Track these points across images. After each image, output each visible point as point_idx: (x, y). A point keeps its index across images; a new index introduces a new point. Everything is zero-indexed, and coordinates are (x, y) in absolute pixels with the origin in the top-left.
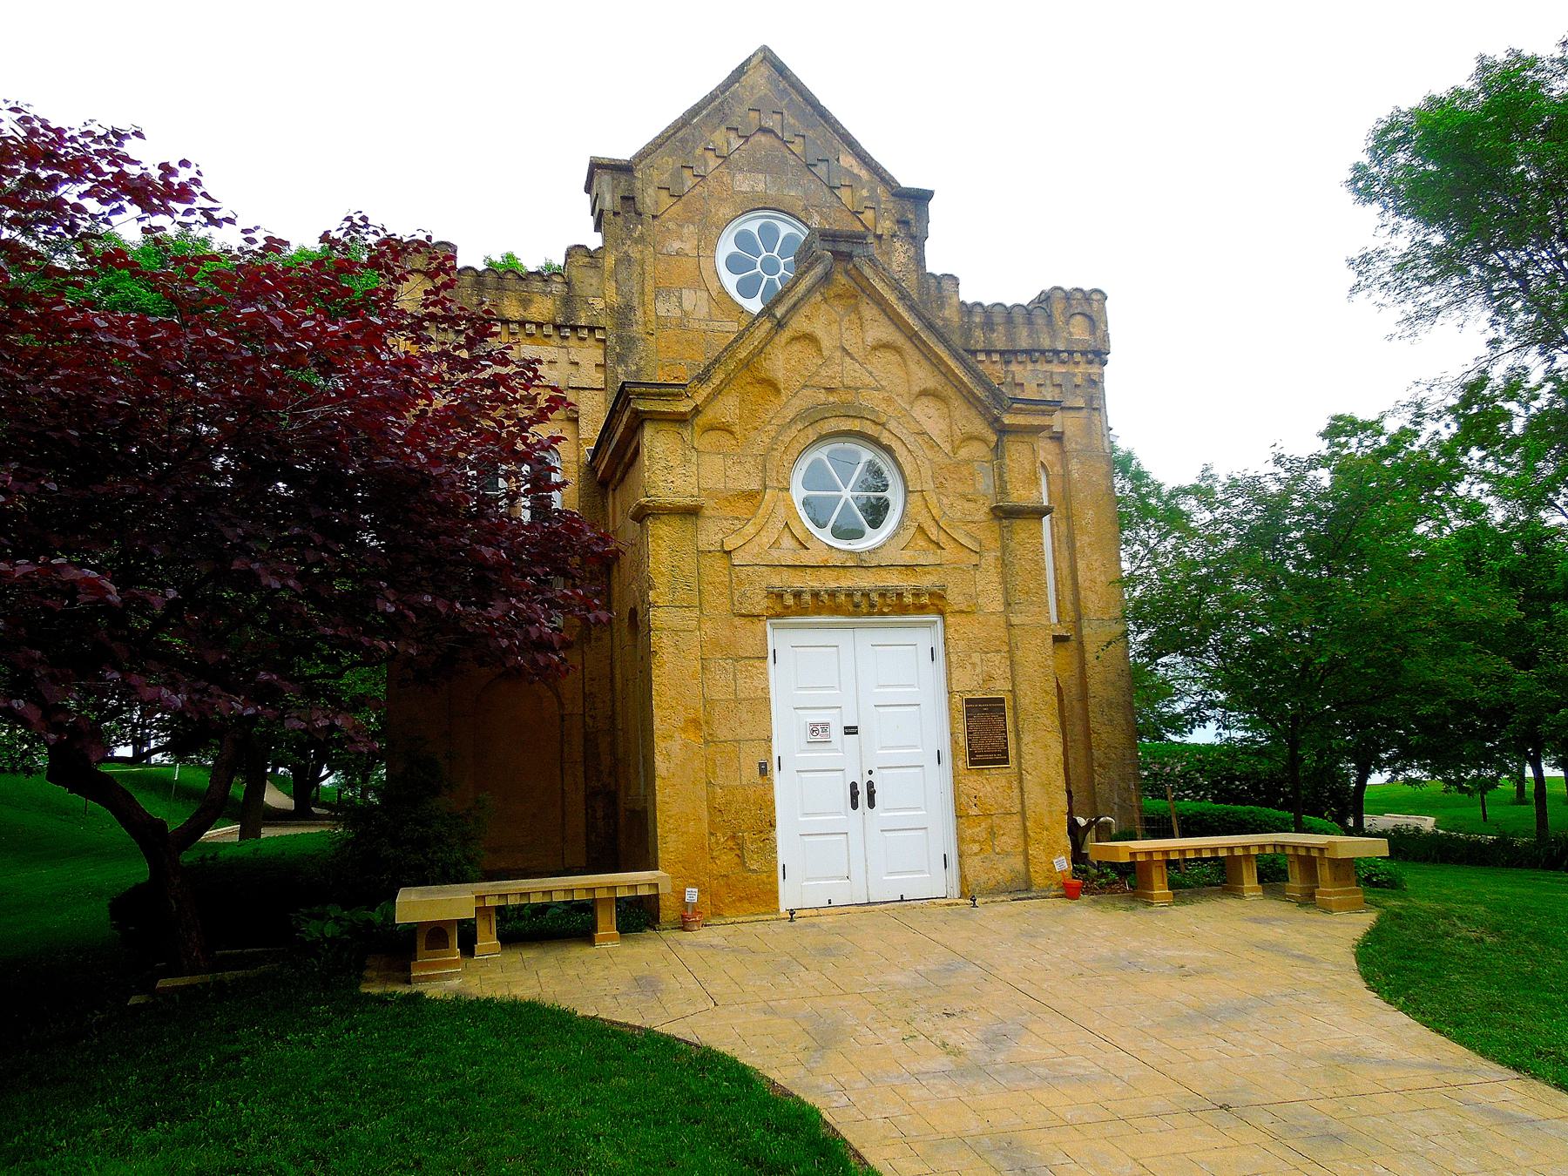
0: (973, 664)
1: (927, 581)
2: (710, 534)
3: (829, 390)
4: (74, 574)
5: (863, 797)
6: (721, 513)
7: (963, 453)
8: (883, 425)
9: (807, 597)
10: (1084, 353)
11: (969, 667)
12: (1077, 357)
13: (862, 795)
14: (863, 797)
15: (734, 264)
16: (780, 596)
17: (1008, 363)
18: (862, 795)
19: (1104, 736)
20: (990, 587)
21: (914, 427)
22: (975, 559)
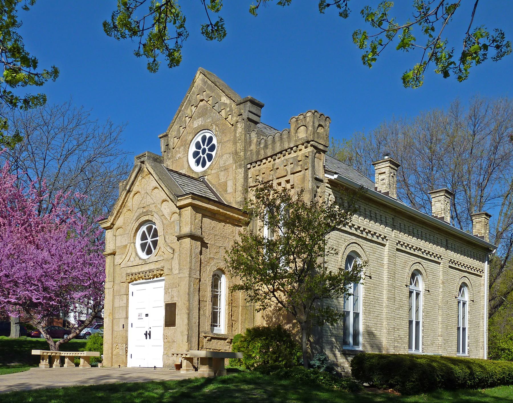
2: (118, 259)
15: (198, 162)
18: (148, 335)
21: (161, 214)
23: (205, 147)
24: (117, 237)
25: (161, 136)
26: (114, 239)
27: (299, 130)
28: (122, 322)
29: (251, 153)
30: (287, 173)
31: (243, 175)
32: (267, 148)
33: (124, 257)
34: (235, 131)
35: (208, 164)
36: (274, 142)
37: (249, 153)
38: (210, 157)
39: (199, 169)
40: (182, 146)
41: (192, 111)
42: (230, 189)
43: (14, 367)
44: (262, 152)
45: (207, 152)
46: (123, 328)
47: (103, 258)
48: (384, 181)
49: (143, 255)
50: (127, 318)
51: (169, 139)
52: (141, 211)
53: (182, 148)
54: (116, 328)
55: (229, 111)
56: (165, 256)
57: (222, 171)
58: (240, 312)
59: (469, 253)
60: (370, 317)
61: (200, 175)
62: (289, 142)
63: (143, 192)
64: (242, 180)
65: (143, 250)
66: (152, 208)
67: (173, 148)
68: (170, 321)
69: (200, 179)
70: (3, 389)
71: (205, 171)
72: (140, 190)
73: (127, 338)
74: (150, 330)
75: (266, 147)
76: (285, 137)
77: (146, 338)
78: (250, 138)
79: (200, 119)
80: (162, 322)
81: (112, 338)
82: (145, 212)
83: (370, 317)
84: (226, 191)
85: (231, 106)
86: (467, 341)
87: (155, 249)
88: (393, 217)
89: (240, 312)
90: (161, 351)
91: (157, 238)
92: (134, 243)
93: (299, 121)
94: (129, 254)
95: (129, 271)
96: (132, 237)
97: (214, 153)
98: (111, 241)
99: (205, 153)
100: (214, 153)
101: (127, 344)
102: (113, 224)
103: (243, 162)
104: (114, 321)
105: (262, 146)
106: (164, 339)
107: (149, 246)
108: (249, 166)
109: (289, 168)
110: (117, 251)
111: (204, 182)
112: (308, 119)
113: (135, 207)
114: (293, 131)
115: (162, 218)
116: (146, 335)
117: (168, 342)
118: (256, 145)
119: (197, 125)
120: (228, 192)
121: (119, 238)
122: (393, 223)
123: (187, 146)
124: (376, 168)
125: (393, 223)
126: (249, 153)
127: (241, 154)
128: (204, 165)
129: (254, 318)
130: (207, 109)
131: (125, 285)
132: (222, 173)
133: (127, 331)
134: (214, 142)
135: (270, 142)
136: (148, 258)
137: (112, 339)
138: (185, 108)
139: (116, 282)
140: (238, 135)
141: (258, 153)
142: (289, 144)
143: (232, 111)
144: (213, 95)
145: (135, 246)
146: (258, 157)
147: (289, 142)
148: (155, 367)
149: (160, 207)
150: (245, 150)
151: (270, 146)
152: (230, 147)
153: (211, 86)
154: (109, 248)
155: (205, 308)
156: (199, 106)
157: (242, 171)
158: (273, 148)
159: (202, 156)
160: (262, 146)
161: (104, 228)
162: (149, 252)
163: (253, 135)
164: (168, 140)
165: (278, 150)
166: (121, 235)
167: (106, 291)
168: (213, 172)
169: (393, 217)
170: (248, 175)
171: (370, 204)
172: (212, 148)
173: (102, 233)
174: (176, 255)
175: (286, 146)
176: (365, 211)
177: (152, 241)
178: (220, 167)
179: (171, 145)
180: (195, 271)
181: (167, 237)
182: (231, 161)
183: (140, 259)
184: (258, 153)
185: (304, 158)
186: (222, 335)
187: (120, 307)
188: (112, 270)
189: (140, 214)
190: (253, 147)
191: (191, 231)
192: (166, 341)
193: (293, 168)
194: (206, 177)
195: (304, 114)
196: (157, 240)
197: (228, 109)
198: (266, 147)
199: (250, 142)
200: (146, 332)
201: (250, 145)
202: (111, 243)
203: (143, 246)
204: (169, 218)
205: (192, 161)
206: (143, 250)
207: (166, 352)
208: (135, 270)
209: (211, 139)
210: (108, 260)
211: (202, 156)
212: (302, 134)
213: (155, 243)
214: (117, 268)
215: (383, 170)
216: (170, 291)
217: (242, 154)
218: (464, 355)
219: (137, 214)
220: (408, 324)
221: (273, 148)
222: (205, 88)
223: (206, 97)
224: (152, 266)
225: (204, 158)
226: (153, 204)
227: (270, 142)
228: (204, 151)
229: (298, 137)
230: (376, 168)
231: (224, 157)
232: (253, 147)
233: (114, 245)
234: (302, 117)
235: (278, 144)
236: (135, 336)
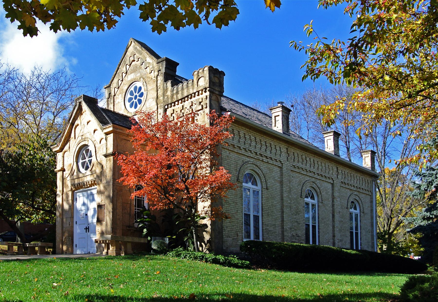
5: (87, 230)
15: (131, 106)
29: (167, 97)
32: (178, 94)
36: (183, 89)
37: (166, 97)
40: (120, 93)
43: (219, 294)
44: (175, 96)
55: (152, 68)
59: (358, 178)
62: (193, 89)
66: (88, 135)
75: (177, 93)
76: (190, 85)
78: (167, 87)
79: (132, 74)
85: (153, 64)
88: (287, 147)
103: (162, 104)
114: (195, 81)
122: (287, 152)
124: (272, 112)
125: (287, 152)
126: (166, 97)
128: (136, 107)
130: (137, 67)
134: (142, 90)
143: (154, 68)
144: (141, 56)
146: (172, 100)
147: (193, 89)
151: (180, 92)
153: (139, 51)
158: (182, 94)
160: (175, 92)
161: (55, 151)
165: (185, 94)
169: (287, 147)
171: (281, 143)
172: (141, 95)
175: (191, 92)
176: (261, 142)
177: (89, 160)
190: (169, 93)
197: (151, 67)
199: (167, 89)
201: (167, 92)
209: (140, 88)
221: (182, 94)
222: (135, 52)
225: (136, 102)
228: (136, 97)
230: (272, 112)
232: (169, 93)
235: (185, 91)
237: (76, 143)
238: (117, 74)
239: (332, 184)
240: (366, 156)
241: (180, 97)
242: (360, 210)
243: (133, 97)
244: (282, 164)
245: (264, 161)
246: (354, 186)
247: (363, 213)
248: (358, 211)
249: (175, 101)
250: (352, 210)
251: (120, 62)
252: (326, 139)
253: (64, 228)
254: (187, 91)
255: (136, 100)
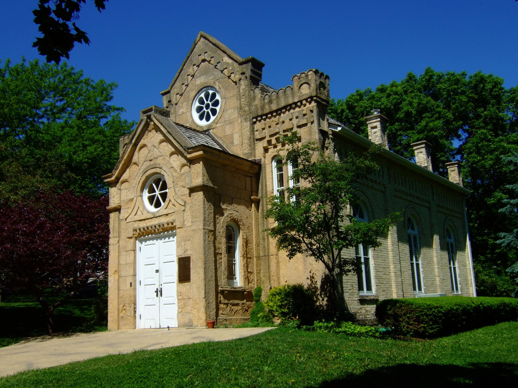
0: (182, 246)
1: (169, 219)
2: (124, 214)
3: (151, 160)
4: (504, 196)
5: (159, 293)
6: (126, 207)
7: (183, 171)
8: (161, 168)
9: (142, 230)
10: (306, 100)
11: (181, 247)
12: (304, 102)
13: (159, 292)
14: (159, 293)
15: (201, 118)
16: (136, 230)
17: (280, 115)
18: (159, 292)
19: (314, 266)
20: (188, 217)
21: (170, 166)
22: (183, 208)
23: (209, 102)
24: (122, 191)
25: (163, 92)
26: (119, 192)
27: (302, 87)
28: (130, 280)
30: (293, 125)
31: (249, 128)
33: (130, 211)
34: (239, 88)
35: (213, 118)
37: (253, 108)
38: (214, 112)
39: (203, 123)
41: (193, 70)
42: (236, 141)
44: (267, 107)
45: (211, 107)
46: (131, 286)
47: (107, 213)
48: (376, 134)
49: (152, 209)
50: (135, 275)
51: (172, 95)
52: (148, 163)
53: (185, 103)
54: (122, 287)
56: (176, 209)
57: (227, 124)
58: (255, 263)
60: (378, 261)
61: (205, 129)
62: (293, 98)
63: (149, 145)
64: (248, 133)
65: (151, 203)
67: (176, 104)
68: (184, 275)
69: (206, 132)
70: (4, 374)
71: (210, 126)
72: (147, 143)
73: (135, 297)
74: (161, 287)
77: (157, 296)
79: (203, 77)
80: (175, 277)
81: (118, 298)
82: (152, 165)
83: (378, 261)
84: (233, 144)
86: (458, 279)
87: (164, 201)
89: (255, 263)
90: (175, 309)
91: (167, 191)
92: (142, 196)
93: (302, 79)
94: (136, 208)
95: (137, 225)
96: (139, 190)
97: (218, 108)
98: (116, 196)
99: (208, 108)
100: (218, 108)
101: (135, 304)
102: (118, 179)
104: (121, 280)
105: (266, 101)
106: (178, 296)
107: (158, 198)
108: (254, 120)
109: (295, 122)
110: (122, 205)
111: (209, 135)
112: (310, 77)
113: (142, 160)
114: (296, 88)
115: (171, 170)
116: (157, 292)
117: (181, 298)
118: (261, 100)
119: (199, 83)
120: (235, 144)
121: (124, 192)
123: (191, 102)
127: (246, 108)
128: (208, 119)
129: (269, 268)
131: (132, 240)
132: (228, 127)
133: (135, 289)
134: (218, 97)
135: (274, 98)
136: (158, 211)
137: (118, 300)
138: (187, 67)
139: (122, 237)
140: (241, 91)
141: (263, 108)
142: (293, 100)
143: (235, 70)
145: (142, 199)
147: (293, 98)
148: (168, 327)
149: (168, 159)
150: (250, 105)
152: (234, 102)
154: (113, 203)
155: (221, 261)
156: (200, 66)
157: (248, 124)
158: (278, 103)
159: (206, 111)
160: (266, 101)
162: (158, 205)
163: (258, 91)
164: (170, 96)
165: (283, 104)
166: (126, 189)
167: (111, 248)
168: (218, 125)
170: (254, 128)
172: (216, 103)
173: (414, 150)
174: (188, 206)
175: (290, 101)
177: (160, 194)
178: (225, 121)
179: (174, 101)
180: (209, 223)
181: (177, 189)
182: (236, 115)
183: (148, 212)
184: (263, 108)
185: (309, 112)
186: (239, 288)
187: (126, 264)
188: (117, 225)
189: (148, 167)
190: (257, 102)
191: (203, 182)
192: (180, 297)
193: (299, 121)
194: (211, 131)
195: (306, 72)
196: (166, 193)
197: (231, 68)
198: (270, 102)
199: (254, 98)
200: (157, 289)
202: (116, 197)
203: (151, 199)
204: (179, 170)
205: (196, 116)
206: (151, 204)
207: (180, 310)
208: (143, 225)
210: (113, 216)
211: (206, 111)
212: (306, 91)
213: (164, 196)
214: (123, 223)
215: (375, 124)
216: (183, 244)
217: (247, 108)
218: (457, 293)
219: (144, 167)
220: (410, 266)
223: (208, 57)
224: (163, 220)
225: (208, 112)
226: (161, 156)
227: (274, 98)
228: (207, 106)
229: (301, 93)
231: (229, 112)
232: (257, 102)
233: (118, 199)
234: (303, 75)
236: (144, 295)
237: (141, 171)
238: (180, 77)
239: (429, 208)
240: (452, 169)
241: (274, 107)
242: (455, 239)
243: (204, 106)
244: (385, 187)
245: (370, 185)
246: (448, 209)
247: (458, 241)
248: (416, 232)
249: (267, 112)
250: (410, 231)
251: (185, 61)
252: (416, 152)
253: (121, 292)
254: (285, 100)
255: (209, 110)
